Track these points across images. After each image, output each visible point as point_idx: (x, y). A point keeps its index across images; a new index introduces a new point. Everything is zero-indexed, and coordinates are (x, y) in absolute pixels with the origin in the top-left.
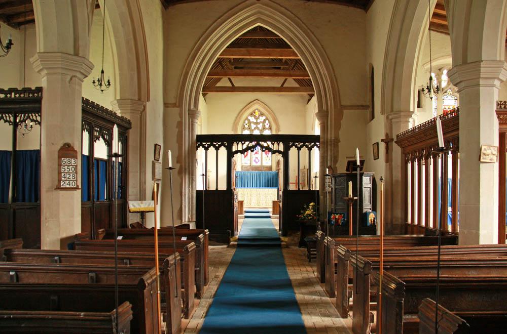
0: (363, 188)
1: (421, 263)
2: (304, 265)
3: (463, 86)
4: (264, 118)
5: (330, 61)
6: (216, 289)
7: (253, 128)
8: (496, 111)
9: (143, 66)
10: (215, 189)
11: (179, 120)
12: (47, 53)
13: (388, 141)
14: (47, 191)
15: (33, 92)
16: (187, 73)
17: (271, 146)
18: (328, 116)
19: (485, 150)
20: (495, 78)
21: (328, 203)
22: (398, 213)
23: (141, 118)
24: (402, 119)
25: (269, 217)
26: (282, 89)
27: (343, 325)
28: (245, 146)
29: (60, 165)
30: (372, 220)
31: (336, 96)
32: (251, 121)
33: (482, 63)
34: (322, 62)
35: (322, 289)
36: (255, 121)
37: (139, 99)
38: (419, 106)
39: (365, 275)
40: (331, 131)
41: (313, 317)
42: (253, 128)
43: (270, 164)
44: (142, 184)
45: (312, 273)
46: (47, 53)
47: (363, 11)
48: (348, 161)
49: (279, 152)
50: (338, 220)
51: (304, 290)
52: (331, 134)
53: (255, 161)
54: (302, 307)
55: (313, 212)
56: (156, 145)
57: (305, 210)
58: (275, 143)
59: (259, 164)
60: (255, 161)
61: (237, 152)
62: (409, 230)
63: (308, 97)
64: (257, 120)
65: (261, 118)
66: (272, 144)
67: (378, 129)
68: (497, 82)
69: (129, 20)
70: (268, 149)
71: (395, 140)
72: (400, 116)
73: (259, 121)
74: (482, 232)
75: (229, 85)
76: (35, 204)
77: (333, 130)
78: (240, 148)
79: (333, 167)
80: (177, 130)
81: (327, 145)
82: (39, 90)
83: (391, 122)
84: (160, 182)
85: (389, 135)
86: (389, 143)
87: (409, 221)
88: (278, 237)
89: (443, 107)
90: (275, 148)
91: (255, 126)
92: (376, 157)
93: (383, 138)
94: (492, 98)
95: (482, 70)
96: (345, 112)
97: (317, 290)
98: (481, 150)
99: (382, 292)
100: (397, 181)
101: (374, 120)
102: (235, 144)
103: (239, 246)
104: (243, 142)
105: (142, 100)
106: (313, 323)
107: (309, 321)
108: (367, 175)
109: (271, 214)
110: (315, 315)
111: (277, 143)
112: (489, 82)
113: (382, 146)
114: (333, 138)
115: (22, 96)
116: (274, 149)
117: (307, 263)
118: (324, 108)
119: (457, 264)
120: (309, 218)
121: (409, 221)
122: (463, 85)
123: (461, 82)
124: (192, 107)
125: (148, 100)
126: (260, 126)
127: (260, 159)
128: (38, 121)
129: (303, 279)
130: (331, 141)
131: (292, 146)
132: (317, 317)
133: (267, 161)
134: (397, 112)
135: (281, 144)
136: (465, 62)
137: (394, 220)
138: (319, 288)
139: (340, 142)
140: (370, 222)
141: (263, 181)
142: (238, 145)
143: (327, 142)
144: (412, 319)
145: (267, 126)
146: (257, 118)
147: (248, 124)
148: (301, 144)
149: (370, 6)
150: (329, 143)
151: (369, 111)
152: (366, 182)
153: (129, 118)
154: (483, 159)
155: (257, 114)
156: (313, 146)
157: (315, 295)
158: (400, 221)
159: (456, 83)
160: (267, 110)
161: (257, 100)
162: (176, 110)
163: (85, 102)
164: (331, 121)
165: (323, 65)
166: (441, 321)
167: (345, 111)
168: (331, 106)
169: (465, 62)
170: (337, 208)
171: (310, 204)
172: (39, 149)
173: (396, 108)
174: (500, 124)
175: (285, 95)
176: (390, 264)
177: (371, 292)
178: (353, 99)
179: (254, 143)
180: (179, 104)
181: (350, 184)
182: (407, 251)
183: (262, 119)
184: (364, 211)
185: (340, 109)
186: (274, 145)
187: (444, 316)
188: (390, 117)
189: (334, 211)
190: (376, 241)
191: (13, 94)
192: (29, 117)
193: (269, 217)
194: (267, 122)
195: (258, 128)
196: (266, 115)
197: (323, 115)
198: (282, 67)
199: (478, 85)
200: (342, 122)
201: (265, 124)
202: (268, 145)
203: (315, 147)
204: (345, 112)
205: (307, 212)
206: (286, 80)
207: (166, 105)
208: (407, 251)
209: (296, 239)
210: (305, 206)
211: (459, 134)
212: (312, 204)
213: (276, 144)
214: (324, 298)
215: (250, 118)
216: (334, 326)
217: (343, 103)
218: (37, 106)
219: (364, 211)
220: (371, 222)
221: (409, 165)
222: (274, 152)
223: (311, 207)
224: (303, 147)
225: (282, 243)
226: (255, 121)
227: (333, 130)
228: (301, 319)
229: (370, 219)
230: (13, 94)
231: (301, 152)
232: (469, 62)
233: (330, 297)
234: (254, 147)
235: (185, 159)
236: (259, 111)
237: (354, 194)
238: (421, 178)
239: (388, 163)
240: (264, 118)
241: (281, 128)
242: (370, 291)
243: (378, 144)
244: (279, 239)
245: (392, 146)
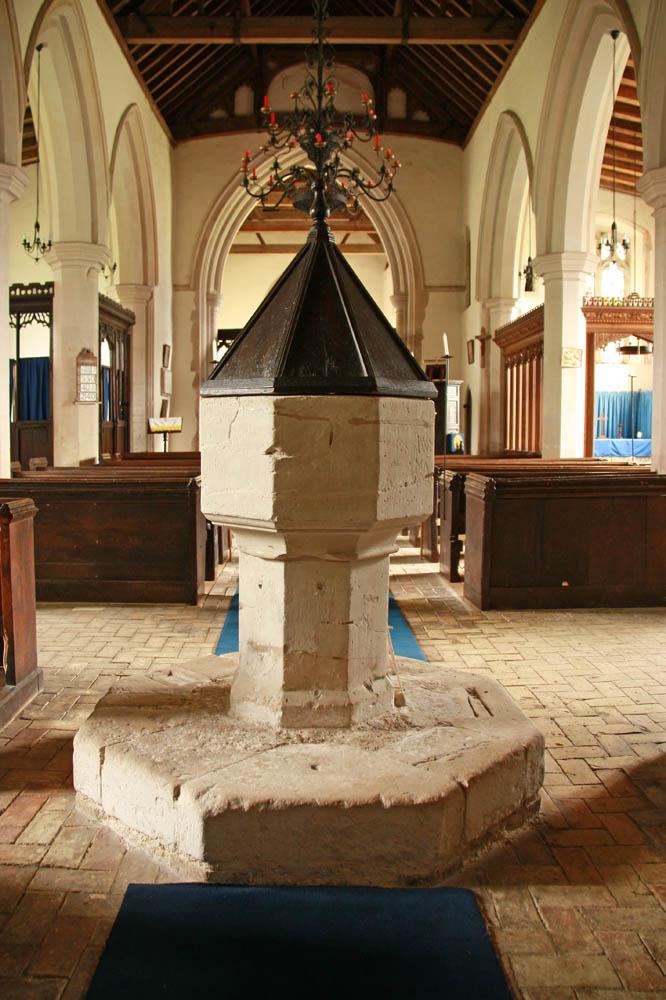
5: (411, 223)
9: (150, 237)
11: (194, 308)
12: (65, 242)
14: (65, 404)
15: (42, 288)
16: (205, 241)
22: (496, 437)
23: (147, 308)
24: (504, 309)
29: (78, 375)
31: (419, 273)
37: (145, 284)
44: (149, 399)
46: (65, 242)
47: (458, 148)
56: (165, 346)
69: (134, 177)
71: (493, 337)
75: (258, 242)
76: (44, 422)
80: (191, 323)
82: (50, 285)
84: (168, 398)
85: (486, 330)
87: (508, 448)
92: (471, 361)
95: (564, 262)
96: (432, 296)
98: (561, 353)
100: (495, 393)
101: (470, 307)
105: (149, 283)
106: (582, 799)
112: (573, 275)
113: (478, 344)
115: (46, 291)
118: (402, 288)
124: (212, 289)
125: (156, 284)
128: (45, 322)
134: (494, 298)
136: (548, 252)
137: (491, 446)
149: (469, 140)
152: (453, 395)
153: (132, 309)
162: (191, 295)
163: (103, 299)
172: (47, 355)
173: (495, 293)
174: (588, 323)
180: (194, 286)
184: (448, 432)
185: (424, 291)
191: (18, 290)
192: (34, 317)
199: (561, 279)
200: (427, 309)
204: (432, 296)
206: (347, 235)
207: (176, 287)
218: (48, 304)
219: (448, 432)
221: (509, 370)
230: (18, 290)
235: (203, 364)
243: (473, 342)
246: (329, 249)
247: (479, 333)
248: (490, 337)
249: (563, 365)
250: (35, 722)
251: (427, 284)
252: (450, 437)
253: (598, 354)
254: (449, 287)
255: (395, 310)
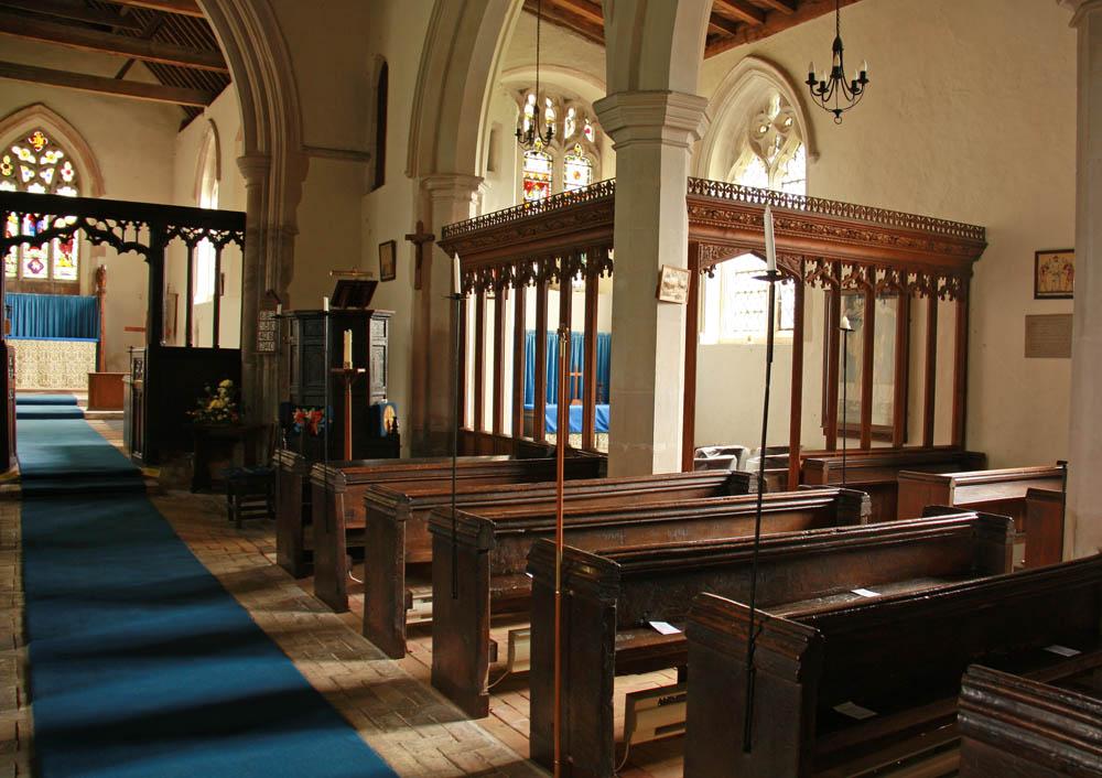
0: (371, 348)
1: (588, 519)
2: (228, 537)
3: (629, 137)
4: (59, 154)
6: (19, 620)
7: (26, 178)
8: (687, 198)
10: (210, 345)
13: (421, 239)
17: (117, 232)
18: (269, 168)
19: (668, 276)
20: (688, 130)
21: (271, 388)
22: (443, 408)
25: (80, 416)
26: (118, 84)
27: (404, 675)
28: (44, 225)
30: (391, 424)
32: (21, 158)
33: (669, 96)
34: (263, 35)
35: (305, 594)
36: (32, 160)
38: (490, 168)
39: (481, 552)
40: (277, 206)
41: (323, 664)
42: (26, 178)
43: (75, 278)
45: (263, 553)
48: (339, 281)
49: (140, 249)
50: (312, 421)
51: (262, 601)
52: (276, 213)
53: (30, 266)
54: (282, 643)
55: (230, 403)
57: (208, 397)
58: (127, 224)
59: (43, 275)
60: (30, 266)
61: (19, 240)
62: (470, 443)
63: (183, 116)
64: (38, 160)
65: (49, 153)
66: (119, 224)
67: (396, 210)
68: (690, 139)
70: (108, 236)
71: (438, 238)
72: (454, 184)
73: (44, 161)
74: (658, 447)
77: (282, 204)
78: (28, 231)
79: (278, 292)
81: (265, 243)
83: (431, 196)
85: (426, 227)
86: (425, 246)
88: (132, 466)
89: (525, 175)
90: (129, 235)
91: (32, 174)
92: (390, 274)
93: (409, 233)
94: (682, 170)
95: (669, 109)
97: (293, 596)
99: (560, 590)
101: (384, 187)
102: (13, 217)
103: (25, 497)
104: (37, 215)
106: (331, 678)
107: (319, 675)
108: (378, 318)
109: (84, 409)
110: (324, 658)
111: (135, 224)
112: (678, 136)
113: (406, 252)
114: (281, 223)
116: (126, 241)
117: (233, 532)
118: (261, 145)
119: (654, 517)
120: (219, 418)
121: (470, 424)
122: (626, 135)
123: (625, 127)
126: (48, 176)
127: (45, 262)
129: (243, 573)
130: (276, 230)
131: (172, 236)
132: (331, 664)
133: (65, 270)
134: (445, 171)
135: (145, 228)
136: (633, 88)
137: (433, 422)
138: (296, 591)
139: (298, 233)
140: (386, 427)
141: (55, 318)
142: (137, 230)
143: (265, 231)
144: (627, 641)
145: (68, 178)
146: (38, 155)
147: (11, 167)
148: (196, 232)
150: (270, 234)
151: (368, 167)
154: (664, 294)
155: (39, 141)
156: (199, 237)
157: (298, 610)
158: (446, 424)
159: (612, 128)
160: (69, 135)
161: (39, 103)
164: (278, 180)
165: (266, 44)
166: (760, 636)
167: (311, 160)
168: (279, 145)
169: (633, 88)
170: (308, 393)
171: (222, 384)
174: (691, 224)
175: (94, 94)
176: (526, 523)
177: (493, 593)
178: (339, 132)
179: (71, 220)
181: (349, 336)
182: (526, 494)
183: (53, 157)
184: (373, 401)
185: (300, 156)
186: (124, 229)
187: (764, 625)
188: (430, 185)
189: (297, 401)
190: (436, 473)
193: (80, 416)
194: (68, 166)
195: (42, 182)
196: (66, 147)
197: (256, 163)
198: (116, 27)
201: (63, 172)
202: (110, 229)
203: (206, 239)
204: (316, 164)
205: (213, 404)
206: (131, 61)
208: (526, 494)
209: (181, 470)
210: (208, 388)
211: (612, 236)
212: (226, 383)
213: (131, 227)
214: (322, 615)
215: (16, 150)
216: (384, 680)
217: (309, 141)
219: (373, 401)
220: (389, 427)
222: (123, 247)
223: (223, 391)
224: (228, 242)
225: (149, 483)
226: (32, 160)
227: (282, 204)
228: (297, 673)
229: (385, 420)
231: (223, 251)
232: (641, 88)
233: (337, 612)
234: (70, 230)
236: (45, 134)
237: (357, 364)
238: (501, 328)
239: (420, 292)
240: (59, 154)
241: (108, 186)
242: (490, 590)
243: (393, 244)
244: (138, 474)
245: (430, 251)
246: (170, 19)
247: (411, 229)
248: (432, 238)
249: (662, 298)
250: (110, 74)
251: (307, 142)
252: (377, 411)
253: (709, 286)
254: (337, 151)
255: (245, 182)
